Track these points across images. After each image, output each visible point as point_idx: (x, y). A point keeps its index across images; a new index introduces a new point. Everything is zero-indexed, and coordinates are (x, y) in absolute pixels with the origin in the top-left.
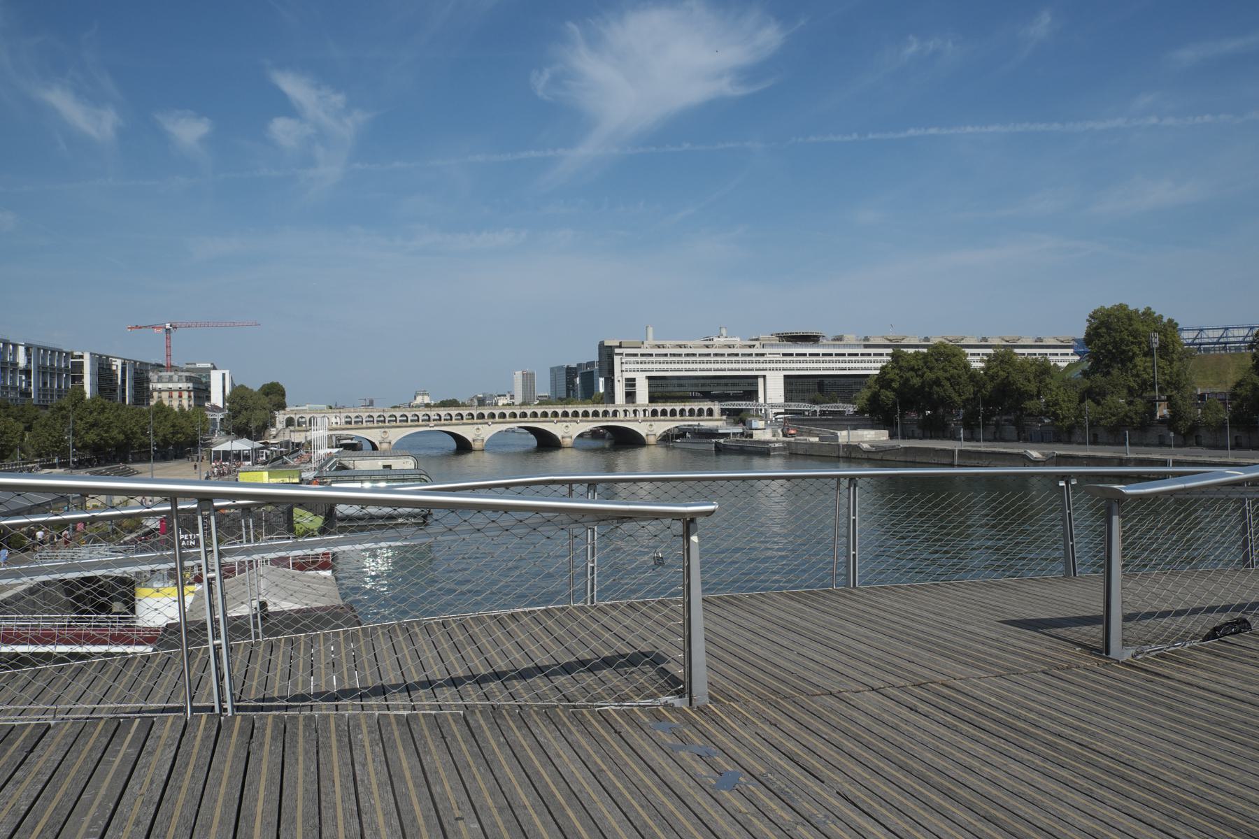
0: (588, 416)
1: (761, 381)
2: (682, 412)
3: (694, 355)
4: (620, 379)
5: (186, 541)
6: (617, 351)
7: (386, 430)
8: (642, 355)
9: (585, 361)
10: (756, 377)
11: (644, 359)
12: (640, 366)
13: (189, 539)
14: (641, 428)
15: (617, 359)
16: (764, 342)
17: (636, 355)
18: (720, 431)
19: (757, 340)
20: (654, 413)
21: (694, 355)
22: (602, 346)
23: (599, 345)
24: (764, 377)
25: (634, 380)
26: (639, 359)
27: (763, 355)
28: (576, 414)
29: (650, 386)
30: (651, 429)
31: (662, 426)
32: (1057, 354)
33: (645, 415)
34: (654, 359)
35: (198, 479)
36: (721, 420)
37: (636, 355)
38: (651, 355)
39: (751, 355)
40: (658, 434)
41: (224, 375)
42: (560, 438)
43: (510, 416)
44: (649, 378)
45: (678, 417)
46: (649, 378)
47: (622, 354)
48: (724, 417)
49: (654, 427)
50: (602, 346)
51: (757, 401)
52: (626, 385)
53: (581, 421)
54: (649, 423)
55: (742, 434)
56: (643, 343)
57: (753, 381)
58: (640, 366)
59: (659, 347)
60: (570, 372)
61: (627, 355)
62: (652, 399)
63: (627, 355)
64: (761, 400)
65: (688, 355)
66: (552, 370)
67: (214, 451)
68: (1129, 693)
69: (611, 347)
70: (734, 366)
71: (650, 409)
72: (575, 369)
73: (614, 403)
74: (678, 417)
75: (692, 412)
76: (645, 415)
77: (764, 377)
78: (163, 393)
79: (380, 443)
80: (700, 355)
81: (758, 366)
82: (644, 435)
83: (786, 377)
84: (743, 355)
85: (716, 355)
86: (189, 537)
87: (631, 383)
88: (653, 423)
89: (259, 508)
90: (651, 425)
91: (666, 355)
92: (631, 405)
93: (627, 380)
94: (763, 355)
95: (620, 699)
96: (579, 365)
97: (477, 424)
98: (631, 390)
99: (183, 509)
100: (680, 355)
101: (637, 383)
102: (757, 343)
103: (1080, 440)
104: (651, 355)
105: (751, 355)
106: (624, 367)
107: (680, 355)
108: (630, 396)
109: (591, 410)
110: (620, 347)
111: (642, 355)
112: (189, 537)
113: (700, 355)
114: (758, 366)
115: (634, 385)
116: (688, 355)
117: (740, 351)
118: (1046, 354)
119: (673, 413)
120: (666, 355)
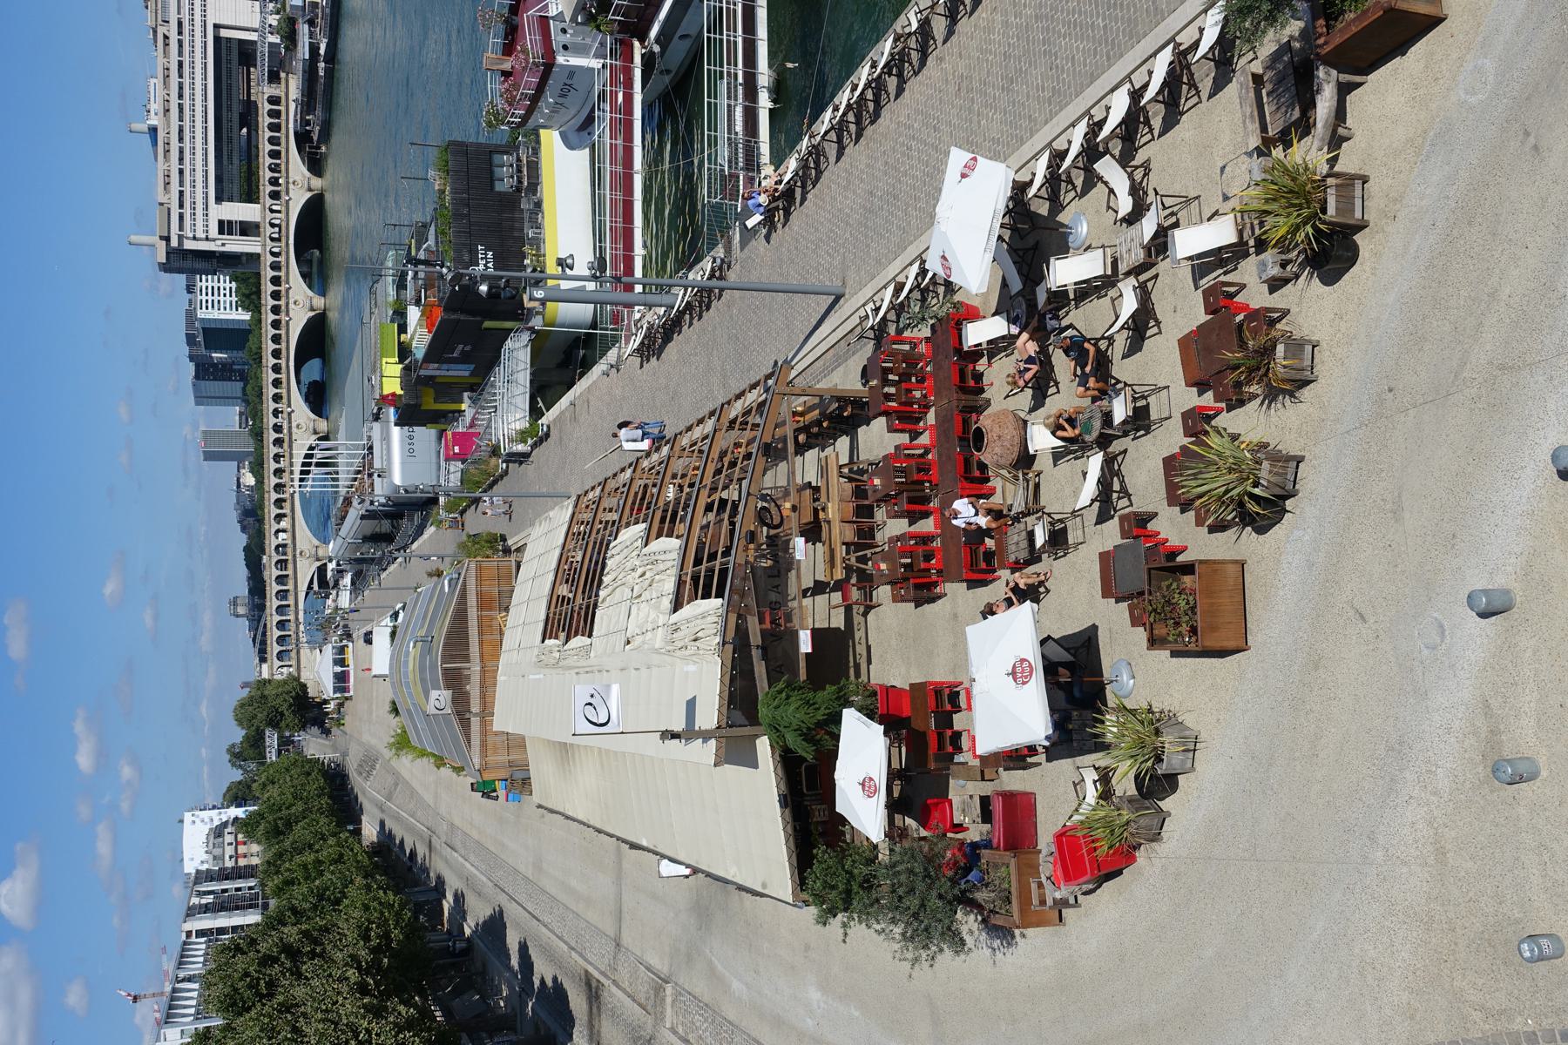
0: (279, 306)
1: (224, 33)
2: (272, 141)
3: (181, 130)
4: (219, 243)
5: (487, 262)
6: (174, 243)
7: (298, 552)
8: (181, 206)
9: (186, 350)
10: (217, 39)
11: (187, 204)
13: (486, 258)
14: (298, 200)
15: (189, 245)
16: (160, 22)
17: (181, 217)
18: (307, 57)
19: (155, 32)
20: (275, 196)
21: (181, 130)
22: (166, 268)
23: (166, 271)
24: (217, 27)
25: (221, 223)
26: (187, 211)
27: (180, 24)
28: (276, 295)
29: (231, 200)
30: (299, 184)
31: (297, 167)
33: (279, 212)
34: (187, 189)
36: (287, 81)
37: (181, 217)
38: (181, 193)
39: (180, 43)
40: (308, 174)
42: (312, 314)
43: (278, 462)
44: (219, 200)
45: (282, 259)
46: (219, 200)
47: (181, 238)
48: (283, 75)
49: (297, 178)
50: (166, 268)
51: (255, 42)
52: (230, 233)
53: (287, 314)
54: (291, 186)
55: (311, 23)
56: (161, 204)
57: (224, 42)
59: (168, 110)
60: (204, 371)
61: (181, 228)
62: (250, 196)
63: (181, 228)
64: (253, 37)
65: (181, 139)
67: (335, 692)
69: (167, 253)
71: (269, 202)
72: (197, 366)
73: (259, 255)
74: (282, 259)
75: (275, 128)
76: (279, 212)
77: (217, 27)
78: (239, 852)
79: (318, 560)
80: (181, 119)
82: (309, 195)
84: (180, 54)
85: (181, 96)
86: (482, 259)
87: (225, 227)
88: (291, 180)
90: (294, 183)
91: (181, 172)
92: (262, 230)
93: (221, 232)
94: (180, 24)
95: (867, 316)
96: (191, 358)
97: (294, 556)
98: (236, 228)
100: (181, 151)
101: (226, 217)
102: (161, 31)
104: (181, 193)
105: (180, 43)
107: (181, 151)
108: (247, 229)
109: (271, 346)
110: (167, 239)
111: (181, 206)
112: (482, 259)
113: (181, 119)
115: (230, 223)
116: (181, 139)
117: (174, 58)
119: (275, 155)
120: (181, 172)
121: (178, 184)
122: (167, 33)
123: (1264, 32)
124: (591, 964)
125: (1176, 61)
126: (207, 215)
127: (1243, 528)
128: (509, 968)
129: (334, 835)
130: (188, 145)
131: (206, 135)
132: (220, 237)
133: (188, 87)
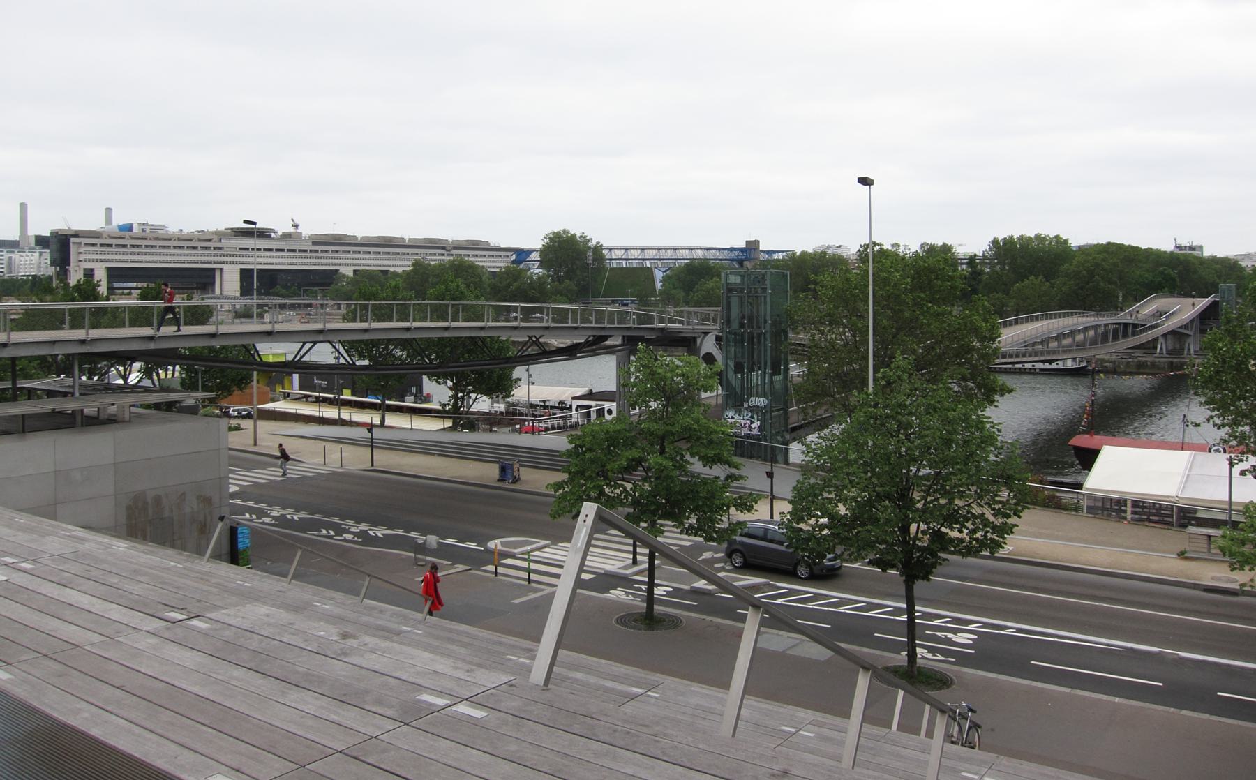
1: (217, 275)
6: (72, 240)
8: (102, 245)
10: (214, 270)
11: (148, 250)
12: (99, 257)
24: (221, 269)
25: (92, 270)
26: (99, 249)
32: (389, 253)
35: (531, 564)
41: (74, 243)
44: (109, 269)
58: (99, 257)
66: (758, 241)
68: (67, 763)
70: (136, 257)
77: (221, 269)
81: (216, 259)
83: (242, 271)
89: (723, 567)
93: (85, 269)
99: (811, 733)
103: (399, 306)
104: (111, 246)
106: (82, 257)
111: (102, 245)
114: (216, 259)
116: (147, 247)
118: (461, 255)
121: (288, 248)
122: (214, 240)
123: (693, 475)
124: (788, 469)
125: (769, 406)
126: (97, 261)
127: (790, 502)
128: (508, 654)
129: (928, 276)
130: (114, 250)
131: (151, 262)
132: (82, 270)
133: (108, 250)
